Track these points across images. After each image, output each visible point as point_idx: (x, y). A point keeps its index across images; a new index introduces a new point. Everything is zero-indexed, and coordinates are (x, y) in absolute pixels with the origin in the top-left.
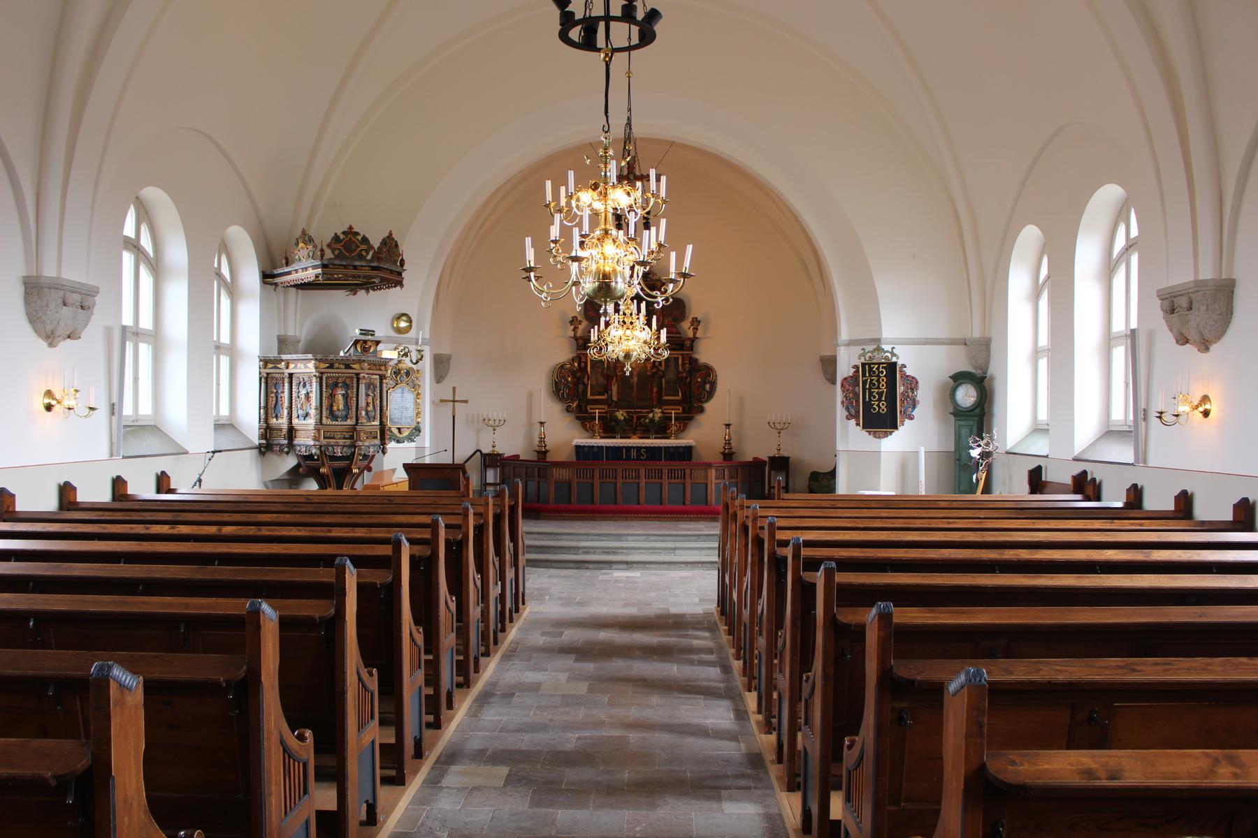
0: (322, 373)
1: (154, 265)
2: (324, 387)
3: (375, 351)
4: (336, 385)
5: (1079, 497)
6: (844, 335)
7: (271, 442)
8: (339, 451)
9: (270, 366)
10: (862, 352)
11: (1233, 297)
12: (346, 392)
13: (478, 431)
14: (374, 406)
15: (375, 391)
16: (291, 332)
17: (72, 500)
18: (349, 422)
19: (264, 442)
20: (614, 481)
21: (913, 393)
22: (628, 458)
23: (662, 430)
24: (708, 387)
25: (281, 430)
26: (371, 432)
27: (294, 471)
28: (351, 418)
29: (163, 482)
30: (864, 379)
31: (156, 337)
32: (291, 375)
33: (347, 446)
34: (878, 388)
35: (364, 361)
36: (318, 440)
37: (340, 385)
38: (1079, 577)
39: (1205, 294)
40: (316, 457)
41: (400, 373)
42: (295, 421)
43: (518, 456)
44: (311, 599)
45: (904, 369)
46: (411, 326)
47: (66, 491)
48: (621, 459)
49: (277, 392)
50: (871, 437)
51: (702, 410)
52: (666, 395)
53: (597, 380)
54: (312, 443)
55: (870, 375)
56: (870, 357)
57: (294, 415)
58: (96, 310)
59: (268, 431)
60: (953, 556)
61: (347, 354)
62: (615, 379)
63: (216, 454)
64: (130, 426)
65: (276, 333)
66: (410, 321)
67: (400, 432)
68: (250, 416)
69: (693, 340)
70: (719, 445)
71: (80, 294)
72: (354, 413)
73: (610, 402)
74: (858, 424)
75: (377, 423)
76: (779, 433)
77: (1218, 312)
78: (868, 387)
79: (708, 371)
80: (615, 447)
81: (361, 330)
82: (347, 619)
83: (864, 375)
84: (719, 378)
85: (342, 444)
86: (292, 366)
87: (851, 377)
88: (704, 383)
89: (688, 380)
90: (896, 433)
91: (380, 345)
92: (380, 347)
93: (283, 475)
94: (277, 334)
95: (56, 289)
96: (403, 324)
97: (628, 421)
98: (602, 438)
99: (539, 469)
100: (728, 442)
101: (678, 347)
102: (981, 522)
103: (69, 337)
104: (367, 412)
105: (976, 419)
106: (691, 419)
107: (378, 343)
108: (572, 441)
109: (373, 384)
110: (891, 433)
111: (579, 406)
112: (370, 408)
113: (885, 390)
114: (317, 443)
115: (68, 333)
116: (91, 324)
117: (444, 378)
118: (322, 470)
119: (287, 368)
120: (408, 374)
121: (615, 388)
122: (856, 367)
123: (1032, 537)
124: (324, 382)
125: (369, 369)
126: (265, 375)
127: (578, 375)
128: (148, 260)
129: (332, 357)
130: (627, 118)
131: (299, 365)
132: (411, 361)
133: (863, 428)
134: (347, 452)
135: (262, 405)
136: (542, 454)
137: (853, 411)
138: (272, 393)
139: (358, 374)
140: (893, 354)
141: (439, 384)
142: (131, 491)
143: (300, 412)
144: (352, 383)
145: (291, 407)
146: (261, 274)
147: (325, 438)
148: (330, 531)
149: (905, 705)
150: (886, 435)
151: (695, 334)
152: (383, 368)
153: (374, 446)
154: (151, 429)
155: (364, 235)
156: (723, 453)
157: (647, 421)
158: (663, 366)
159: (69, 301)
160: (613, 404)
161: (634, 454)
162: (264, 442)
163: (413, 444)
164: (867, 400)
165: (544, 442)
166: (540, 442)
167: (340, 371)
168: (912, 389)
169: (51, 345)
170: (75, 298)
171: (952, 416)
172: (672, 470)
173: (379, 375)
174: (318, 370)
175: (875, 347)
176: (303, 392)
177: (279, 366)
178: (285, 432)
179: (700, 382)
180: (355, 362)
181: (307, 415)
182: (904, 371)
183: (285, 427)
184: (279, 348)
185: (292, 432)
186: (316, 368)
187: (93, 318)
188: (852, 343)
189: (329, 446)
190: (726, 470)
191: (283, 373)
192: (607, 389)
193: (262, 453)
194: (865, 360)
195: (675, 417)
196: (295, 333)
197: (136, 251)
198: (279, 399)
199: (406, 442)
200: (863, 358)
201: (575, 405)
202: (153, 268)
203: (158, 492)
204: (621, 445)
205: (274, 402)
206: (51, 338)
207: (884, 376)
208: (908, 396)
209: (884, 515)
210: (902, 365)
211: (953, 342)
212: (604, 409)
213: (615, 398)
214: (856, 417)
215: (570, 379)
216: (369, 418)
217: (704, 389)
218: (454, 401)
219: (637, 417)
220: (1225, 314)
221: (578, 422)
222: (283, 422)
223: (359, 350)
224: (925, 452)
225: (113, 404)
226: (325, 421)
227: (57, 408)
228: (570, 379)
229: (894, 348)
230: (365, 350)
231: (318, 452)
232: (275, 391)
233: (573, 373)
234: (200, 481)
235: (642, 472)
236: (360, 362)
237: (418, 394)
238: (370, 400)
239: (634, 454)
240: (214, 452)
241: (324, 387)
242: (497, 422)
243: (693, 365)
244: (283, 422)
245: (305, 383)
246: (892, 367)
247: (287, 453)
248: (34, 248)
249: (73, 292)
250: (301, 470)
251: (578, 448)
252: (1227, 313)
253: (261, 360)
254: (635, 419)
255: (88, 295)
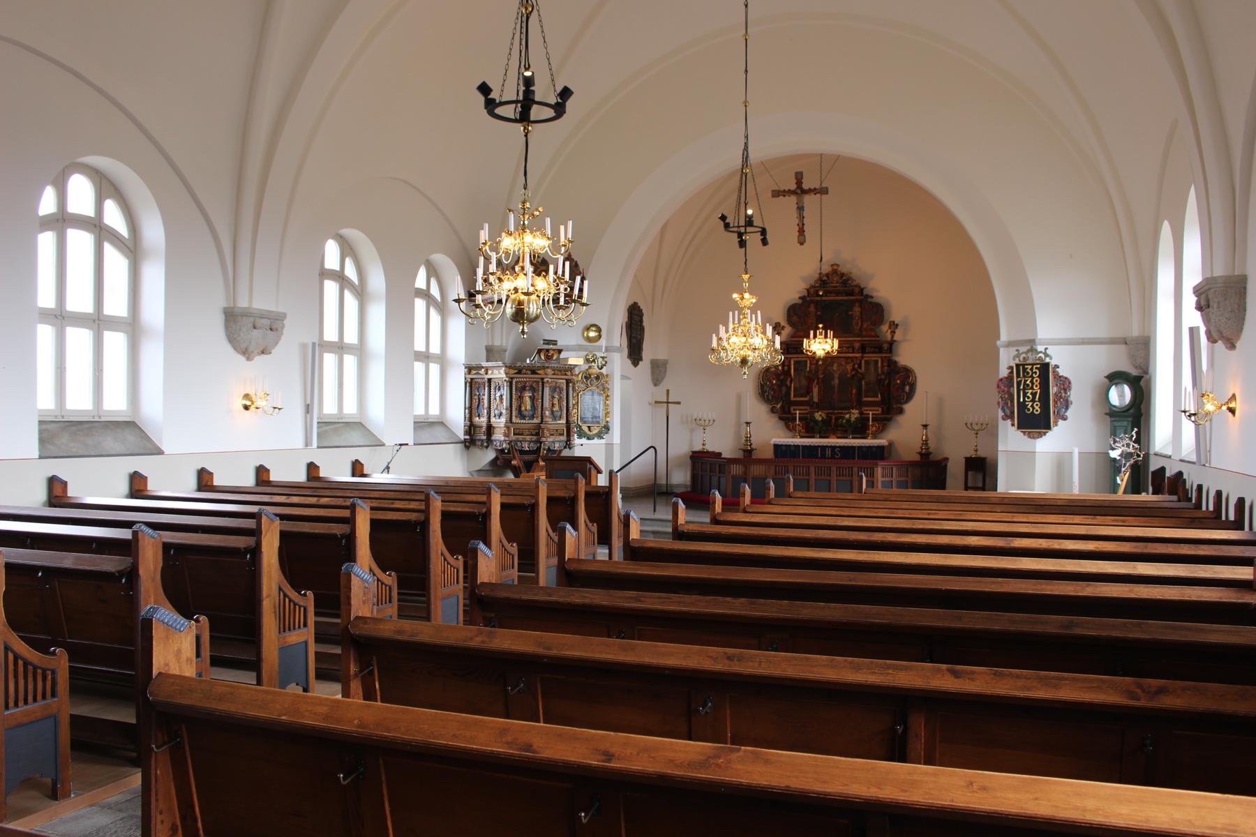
0: (512, 378)
1: (360, 292)
2: (514, 390)
3: (558, 358)
4: (524, 388)
5: (1175, 498)
6: (1004, 337)
7: (474, 437)
8: (527, 446)
9: (473, 372)
10: (1017, 353)
11: (1245, 293)
12: (533, 395)
13: (692, 431)
14: (560, 407)
15: (561, 393)
16: (497, 343)
17: (265, 479)
18: (535, 421)
19: (468, 437)
20: (850, 478)
21: (1066, 393)
22: (823, 456)
23: (860, 429)
24: (907, 388)
25: (481, 427)
26: (557, 430)
27: (494, 462)
28: (537, 417)
29: (357, 469)
30: (1019, 379)
31: (360, 350)
32: (490, 380)
33: (533, 442)
34: (1032, 388)
35: (548, 367)
36: (508, 437)
37: (527, 388)
38: (860, 553)
39: (1216, 291)
40: (506, 451)
41: (590, 377)
42: (493, 420)
43: (720, 454)
44: (881, 626)
45: (1057, 369)
46: (600, 336)
47: (261, 472)
48: (817, 457)
49: (480, 394)
50: (1026, 437)
51: (901, 411)
52: (865, 397)
53: (800, 382)
54: (503, 438)
55: (1024, 376)
56: (1024, 358)
57: (492, 415)
58: (285, 331)
59: (471, 428)
60: (826, 536)
61: (533, 362)
62: (816, 381)
63: (403, 447)
64: (338, 423)
65: (485, 342)
66: (599, 330)
67: (590, 430)
68: (457, 415)
69: (891, 344)
70: (917, 445)
71: (270, 319)
72: (540, 413)
73: (811, 403)
74: (1013, 425)
75: (563, 421)
76: (977, 434)
77: (1229, 310)
78: (1022, 387)
79: (907, 373)
80: (844, 447)
81: (544, 340)
82: (263, 550)
83: (1018, 376)
84: (919, 380)
85: (529, 440)
86: (490, 372)
87: (1007, 378)
88: (903, 385)
89: (886, 382)
90: (1050, 434)
91: (563, 353)
92: (563, 355)
93: (484, 466)
94: (486, 344)
95: (247, 316)
96: (592, 334)
97: (826, 422)
98: (802, 437)
99: (720, 465)
100: (925, 443)
101: (877, 350)
102: (961, 514)
103: (263, 353)
104: (552, 412)
105: (1130, 419)
106: (889, 420)
107: (560, 351)
108: (770, 441)
109: (559, 387)
110: (1045, 434)
111: (782, 407)
112: (556, 408)
113: (1039, 391)
114: (507, 439)
115: (261, 349)
116: (281, 343)
117: (660, 383)
118: (514, 462)
119: (486, 374)
120: (597, 378)
121: (815, 390)
122: (1011, 368)
123: (962, 526)
124: (514, 386)
125: (554, 374)
126: (469, 380)
127: (782, 377)
128: (354, 287)
129: (519, 364)
130: (743, 144)
131: (495, 371)
132: (598, 366)
133: (1018, 428)
134: (534, 446)
135: (467, 406)
136: (748, 452)
137: (1008, 412)
138: (475, 395)
139: (543, 379)
140: (1046, 355)
141: (657, 387)
142: (323, 473)
143: (496, 412)
144: (539, 387)
145: (489, 407)
146: (467, 293)
147: (514, 434)
148: (393, 503)
149: (493, 615)
150: (1040, 435)
151: (893, 337)
152: (569, 373)
153: (560, 442)
154: (358, 425)
155: (543, 258)
156: (920, 454)
157: (844, 421)
158: (863, 368)
159: (258, 325)
160: (815, 405)
161: (828, 453)
162: (468, 437)
163: (603, 441)
164: (1022, 400)
165: (750, 440)
166: (747, 440)
167: (526, 378)
168: (1065, 390)
169: (248, 359)
170: (266, 322)
171: (1108, 417)
172: (840, 468)
173: (566, 380)
174: (508, 375)
175: (1028, 348)
176: (498, 394)
177: (480, 372)
178: (484, 429)
179: (899, 384)
180: (539, 368)
181: (501, 414)
182: (1058, 372)
183: (484, 424)
184: (487, 356)
185: (490, 429)
186: (506, 374)
187: (283, 338)
188: (1010, 344)
189: (518, 441)
190: (894, 469)
191: (484, 378)
192: (809, 391)
193: (467, 447)
194: (1020, 361)
195: (872, 418)
196: (502, 343)
197: (341, 280)
198: (481, 401)
199: (596, 438)
200: (1017, 359)
201: (779, 406)
202: (358, 293)
203: (353, 475)
204: (816, 445)
205: (477, 404)
206: (247, 353)
207: (1038, 377)
208: (1061, 397)
209: (904, 507)
210: (1056, 365)
211: (1112, 341)
212: (806, 410)
213: (816, 400)
214: (1012, 418)
215: (774, 382)
216: (554, 418)
217: (903, 390)
218: (668, 403)
219: (835, 417)
220: (1237, 311)
221: (782, 423)
222: (483, 421)
223: (543, 357)
224: (1079, 453)
225: (308, 405)
226: (514, 420)
227: (252, 408)
228: (774, 382)
229: (1046, 349)
230: (548, 358)
231: (508, 446)
232: (478, 394)
233: (777, 375)
234: (388, 468)
235: (812, 470)
236: (544, 368)
237: (608, 396)
238: (556, 401)
239: (828, 453)
240: (401, 445)
241: (514, 390)
242: (707, 422)
243: (893, 368)
244: (483, 421)
245: (499, 387)
246: (1045, 368)
247: (487, 447)
248: (231, 287)
249: (262, 318)
250: (499, 462)
251: (776, 447)
252: (1239, 310)
253: (466, 368)
254: (833, 421)
255: (277, 320)
